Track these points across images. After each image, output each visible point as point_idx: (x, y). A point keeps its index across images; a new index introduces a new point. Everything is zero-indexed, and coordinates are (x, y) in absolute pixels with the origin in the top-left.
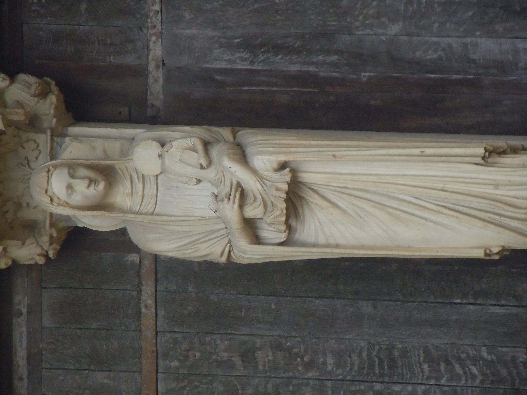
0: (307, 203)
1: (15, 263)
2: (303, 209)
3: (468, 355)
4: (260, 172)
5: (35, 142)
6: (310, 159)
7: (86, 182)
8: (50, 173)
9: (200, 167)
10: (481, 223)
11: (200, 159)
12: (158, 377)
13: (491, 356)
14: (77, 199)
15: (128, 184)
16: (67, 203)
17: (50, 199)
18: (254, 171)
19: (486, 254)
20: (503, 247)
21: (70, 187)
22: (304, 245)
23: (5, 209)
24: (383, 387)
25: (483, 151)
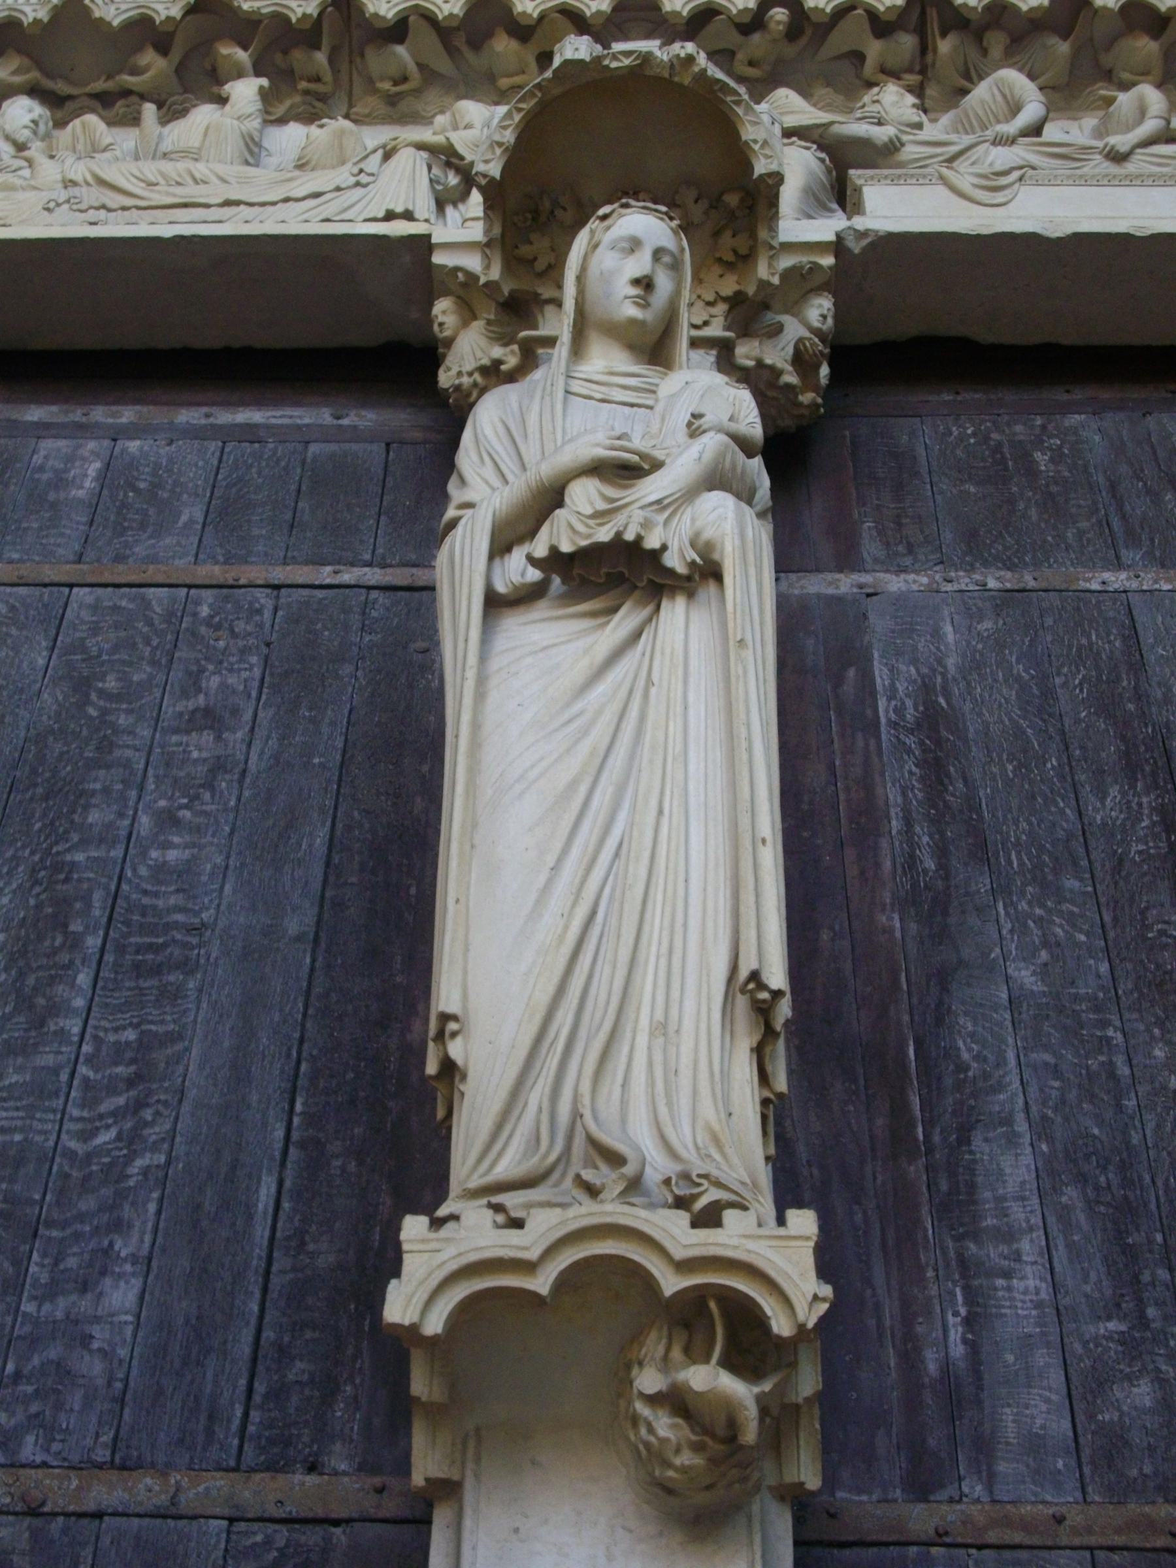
3: (146, 1124)
10: (543, 997)
16: (596, 246)
18: (691, 494)
19: (445, 1018)
20: (464, 1077)
21: (634, 245)
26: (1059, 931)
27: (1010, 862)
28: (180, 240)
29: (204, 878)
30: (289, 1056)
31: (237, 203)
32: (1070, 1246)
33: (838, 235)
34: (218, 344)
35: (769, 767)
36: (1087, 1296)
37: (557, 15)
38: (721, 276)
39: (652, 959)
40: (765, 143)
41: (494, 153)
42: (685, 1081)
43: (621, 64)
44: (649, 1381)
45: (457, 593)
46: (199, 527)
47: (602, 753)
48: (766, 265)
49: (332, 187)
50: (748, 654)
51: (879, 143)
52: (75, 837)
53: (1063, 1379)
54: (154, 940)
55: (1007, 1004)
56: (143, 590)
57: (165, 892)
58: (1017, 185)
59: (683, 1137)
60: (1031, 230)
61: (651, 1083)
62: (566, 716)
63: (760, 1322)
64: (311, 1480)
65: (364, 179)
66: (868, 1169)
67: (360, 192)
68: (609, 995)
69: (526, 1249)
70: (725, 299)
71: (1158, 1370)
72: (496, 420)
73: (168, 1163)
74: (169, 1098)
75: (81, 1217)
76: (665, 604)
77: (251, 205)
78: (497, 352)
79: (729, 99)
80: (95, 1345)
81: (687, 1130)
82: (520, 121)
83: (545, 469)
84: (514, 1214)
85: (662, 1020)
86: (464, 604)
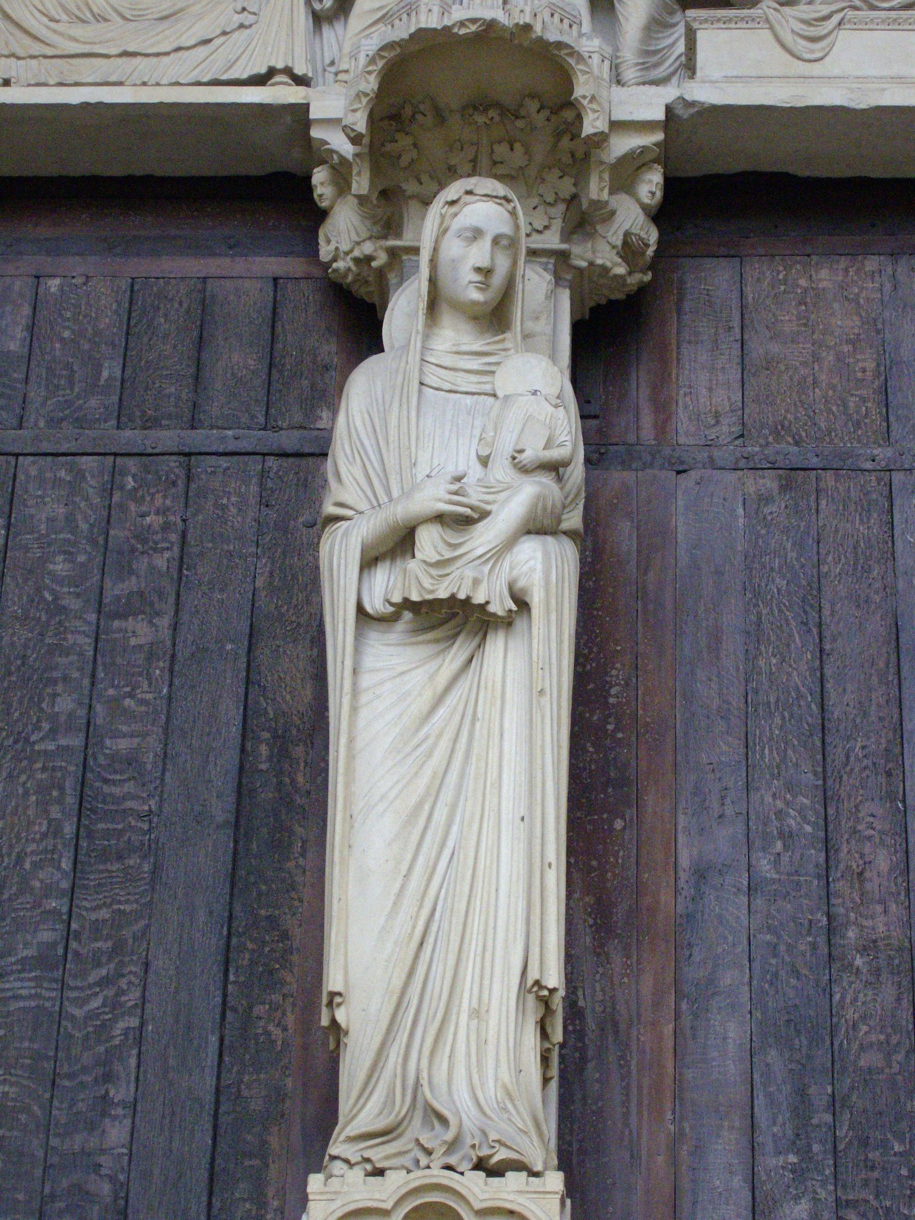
0: (438, 654)
1: (321, 215)
2: (429, 642)
3: (123, 993)
4: (509, 556)
6: (535, 645)
7: (485, 263)
8: (503, 201)
9: (518, 448)
10: (398, 982)
11: (533, 452)
12: (107, 457)
13: (121, 1035)
14: (452, 248)
15: (476, 347)
16: (446, 230)
17: (455, 198)
18: (510, 543)
19: (333, 995)
20: (346, 1033)
21: (476, 234)
22: (357, 651)
23: (425, 178)
24: (68, 836)
25: (551, 986)
26: (793, 822)
28: (86, 105)
29: (149, 767)
30: (221, 933)
32: (769, 1095)
33: (669, 109)
35: (558, 799)
36: (774, 1135)
38: (561, 177)
39: (472, 955)
40: (593, 99)
41: (360, 102)
42: (491, 1048)
43: (468, 31)
45: (336, 602)
46: (118, 384)
47: (441, 775)
48: (597, 180)
49: (218, 32)
52: (46, 726)
53: (750, 1198)
54: (116, 826)
55: (746, 890)
57: (120, 780)
58: (835, 32)
61: (468, 1054)
62: (415, 741)
65: (247, 19)
66: (634, 1033)
68: (441, 991)
69: (384, 1201)
70: (564, 200)
71: (815, 1192)
72: (364, 410)
73: (142, 1024)
74: (138, 971)
75: (85, 1070)
77: (147, 55)
78: (368, 248)
79: (563, 52)
80: (104, 1171)
82: (383, 67)
84: (379, 1165)
85: (476, 1007)
86: (341, 626)
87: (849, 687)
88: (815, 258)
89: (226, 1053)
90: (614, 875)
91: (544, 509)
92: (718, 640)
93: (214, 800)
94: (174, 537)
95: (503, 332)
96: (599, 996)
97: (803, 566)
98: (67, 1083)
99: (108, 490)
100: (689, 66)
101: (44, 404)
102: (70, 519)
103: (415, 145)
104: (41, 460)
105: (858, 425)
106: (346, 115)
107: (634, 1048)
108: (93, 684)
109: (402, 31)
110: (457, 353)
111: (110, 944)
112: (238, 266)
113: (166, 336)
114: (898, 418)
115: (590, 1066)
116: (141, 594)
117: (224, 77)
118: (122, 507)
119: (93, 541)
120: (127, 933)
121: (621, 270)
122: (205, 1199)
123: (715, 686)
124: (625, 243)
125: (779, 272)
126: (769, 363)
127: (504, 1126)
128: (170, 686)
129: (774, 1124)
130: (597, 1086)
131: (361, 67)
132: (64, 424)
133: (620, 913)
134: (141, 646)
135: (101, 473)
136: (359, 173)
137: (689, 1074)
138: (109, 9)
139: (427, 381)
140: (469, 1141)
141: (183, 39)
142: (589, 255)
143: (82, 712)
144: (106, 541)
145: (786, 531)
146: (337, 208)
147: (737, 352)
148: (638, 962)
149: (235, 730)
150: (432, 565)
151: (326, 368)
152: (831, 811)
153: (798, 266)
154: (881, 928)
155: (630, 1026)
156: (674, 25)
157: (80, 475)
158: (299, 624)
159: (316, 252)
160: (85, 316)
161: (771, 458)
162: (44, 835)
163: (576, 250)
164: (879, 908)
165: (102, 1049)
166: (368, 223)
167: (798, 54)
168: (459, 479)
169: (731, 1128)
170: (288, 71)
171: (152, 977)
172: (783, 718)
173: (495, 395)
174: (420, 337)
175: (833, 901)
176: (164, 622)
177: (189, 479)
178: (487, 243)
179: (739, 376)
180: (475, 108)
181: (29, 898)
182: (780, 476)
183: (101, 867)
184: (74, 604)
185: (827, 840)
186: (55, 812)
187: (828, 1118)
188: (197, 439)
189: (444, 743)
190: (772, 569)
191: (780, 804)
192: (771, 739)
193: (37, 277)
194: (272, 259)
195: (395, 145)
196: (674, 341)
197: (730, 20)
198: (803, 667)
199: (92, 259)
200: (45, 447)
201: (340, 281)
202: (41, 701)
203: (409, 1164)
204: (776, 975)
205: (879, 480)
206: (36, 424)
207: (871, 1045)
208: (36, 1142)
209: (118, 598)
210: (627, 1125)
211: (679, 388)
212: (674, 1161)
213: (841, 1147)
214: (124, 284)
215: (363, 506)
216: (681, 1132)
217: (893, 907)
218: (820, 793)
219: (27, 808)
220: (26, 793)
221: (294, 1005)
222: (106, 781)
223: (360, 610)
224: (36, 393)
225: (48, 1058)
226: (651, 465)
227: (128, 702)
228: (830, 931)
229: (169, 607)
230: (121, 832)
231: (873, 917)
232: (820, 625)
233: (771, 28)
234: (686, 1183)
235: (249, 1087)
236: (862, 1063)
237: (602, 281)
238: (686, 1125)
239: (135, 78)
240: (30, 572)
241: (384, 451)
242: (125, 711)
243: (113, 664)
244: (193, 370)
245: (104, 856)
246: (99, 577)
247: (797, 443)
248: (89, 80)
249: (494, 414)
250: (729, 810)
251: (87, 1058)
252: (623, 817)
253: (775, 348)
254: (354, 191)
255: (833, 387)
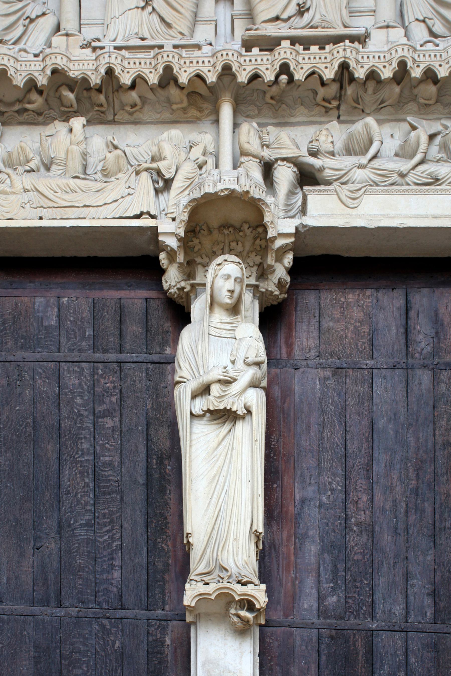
0: (220, 427)
1: (163, 272)
2: (216, 424)
3: (115, 534)
5: (250, 276)
7: (231, 288)
11: (252, 358)
14: (219, 282)
16: (217, 276)
19: (188, 534)
20: (192, 545)
21: (228, 277)
23: (204, 256)
26: (334, 486)
27: (324, 465)
31: (88, 206)
32: (324, 567)
33: (297, 228)
34: (86, 255)
37: (195, 78)
40: (272, 222)
42: (240, 550)
44: (233, 611)
46: (92, 337)
49: (120, 197)
50: (258, 443)
51: (316, 168)
52: (80, 453)
56: (80, 363)
59: (239, 563)
60: (363, 226)
61: (233, 551)
62: (212, 456)
63: (254, 605)
64: (163, 612)
65: (131, 191)
66: (281, 548)
67: (129, 198)
70: (256, 265)
73: (122, 544)
75: (104, 556)
76: (237, 422)
78: (183, 284)
79: (261, 203)
81: (240, 560)
83: (206, 379)
86: (185, 418)
87: (355, 442)
88: (347, 290)
89: (149, 552)
90: (274, 502)
91: (256, 379)
92: (309, 427)
93: (139, 477)
94: (117, 391)
95: (237, 315)
96: (269, 538)
97: (340, 402)
98: (99, 560)
99: (93, 374)
100: (303, 211)
101: (66, 344)
102: (80, 384)
103: (200, 243)
104: (68, 364)
105: (361, 352)
106: (176, 230)
107: (281, 553)
108: (94, 440)
109: (197, 195)
110: (221, 323)
111: (109, 520)
112: (132, 294)
113: (108, 319)
114: (376, 350)
115: (266, 558)
116: (108, 410)
117: (124, 216)
118: (98, 381)
119: (89, 392)
120: (114, 517)
121: (277, 293)
122: (146, 593)
123: (308, 442)
124: (279, 282)
125: (333, 296)
126: (329, 330)
127: (246, 572)
128: (121, 440)
129: (326, 575)
130: (268, 564)
131: (181, 210)
132: (74, 351)
133: (276, 513)
134: (110, 427)
135: (90, 368)
136: (179, 254)
137: (299, 561)
138: (77, 188)
139: (211, 333)
140: (234, 576)
141: (107, 200)
142: (266, 287)
143: (92, 449)
144: (94, 392)
145: (334, 390)
146: (169, 269)
147: (317, 325)
148: (282, 528)
149: (144, 455)
150: (217, 398)
151: (167, 332)
152: (347, 482)
153: (341, 293)
154: (363, 519)
155: (279, 547)
156: (297, 193)
157: (82, 369)
158: (163, 421)
159: (163, 287)
160: (78, 312)
161: (329, 364)
162: (84, 487)
163: (261, 285)
164: (363, 513)
165: (109, 550)
166: (182, 275)
167: (348, 205)
168: (225, 368)
169: (312, 576)
170: (148, 213)
171: (123, 530)
172: (332, 453)
173: (235, 338)
174: (208, 317)
175: (347, 510)
176: (117, 419)
177: (121, 371)
178: (232, 280)
179: (318, 334)
180: (224, 227)
181: (80, 506)
182: (332, 371)
183: (104, 497)
184: (85, 413)
185: (346, 491)
186: (86, 480)
187: (344, 574)
188: (123, 357)
189: (222, 457)
190: (329, 403)
191: (330, 480)
192: (327, 459)
193: (59, 297)
194: (144, 291)
195: (192, 243)
196: (294, 322)
197: (321, 191)
198: (339, 436)
199: (78, 291)
200: (69, 359)
201: (172, 297)
202: (77, 445)
203: (216, 582)
204: (327, 532)
205: (368, 372)
206: (64, 351)
207: (358, 553)
208: (91, 576)
209: (100, 411)
210: (278, 574)
211: (296, 339)
212: (294, 585)
213: (347, 582)
214: (91, 300)
215: (190, 378)
216: (296, 577)
217: (367, 512)
218: (344, 477)
219: (77, 478)
220: (76, 474)
221: (170, 539)
222: (102, 470)
223: (192, 414)
224: (63, 340)
225: (93, 553)
226: (286, 367)
227: (107, 445)
228: (346, 519)
229: (118, 414)
230: (108, 487)
231: (360, 515)
232: (345, 422)
233: (337, 194)
234: (297, 591)
235: (157, 562)
236: (355, 558)
237: (270, 297)
238: (298, 575)
239: (89, 216)
240: (68, 402)
241: (197, 358)
242: (106, 448)
243: (101, 433)
244: (118, 332)
245: (104, 493)
246: (92, 404)
247: (339, 359)
248: (72, 217)
249: (236, 345)
250: (313, 482)
251: (105, 553)
252: (277, 484)
253: (331, 324)
254: (178, 260)
255: (353, 339)
